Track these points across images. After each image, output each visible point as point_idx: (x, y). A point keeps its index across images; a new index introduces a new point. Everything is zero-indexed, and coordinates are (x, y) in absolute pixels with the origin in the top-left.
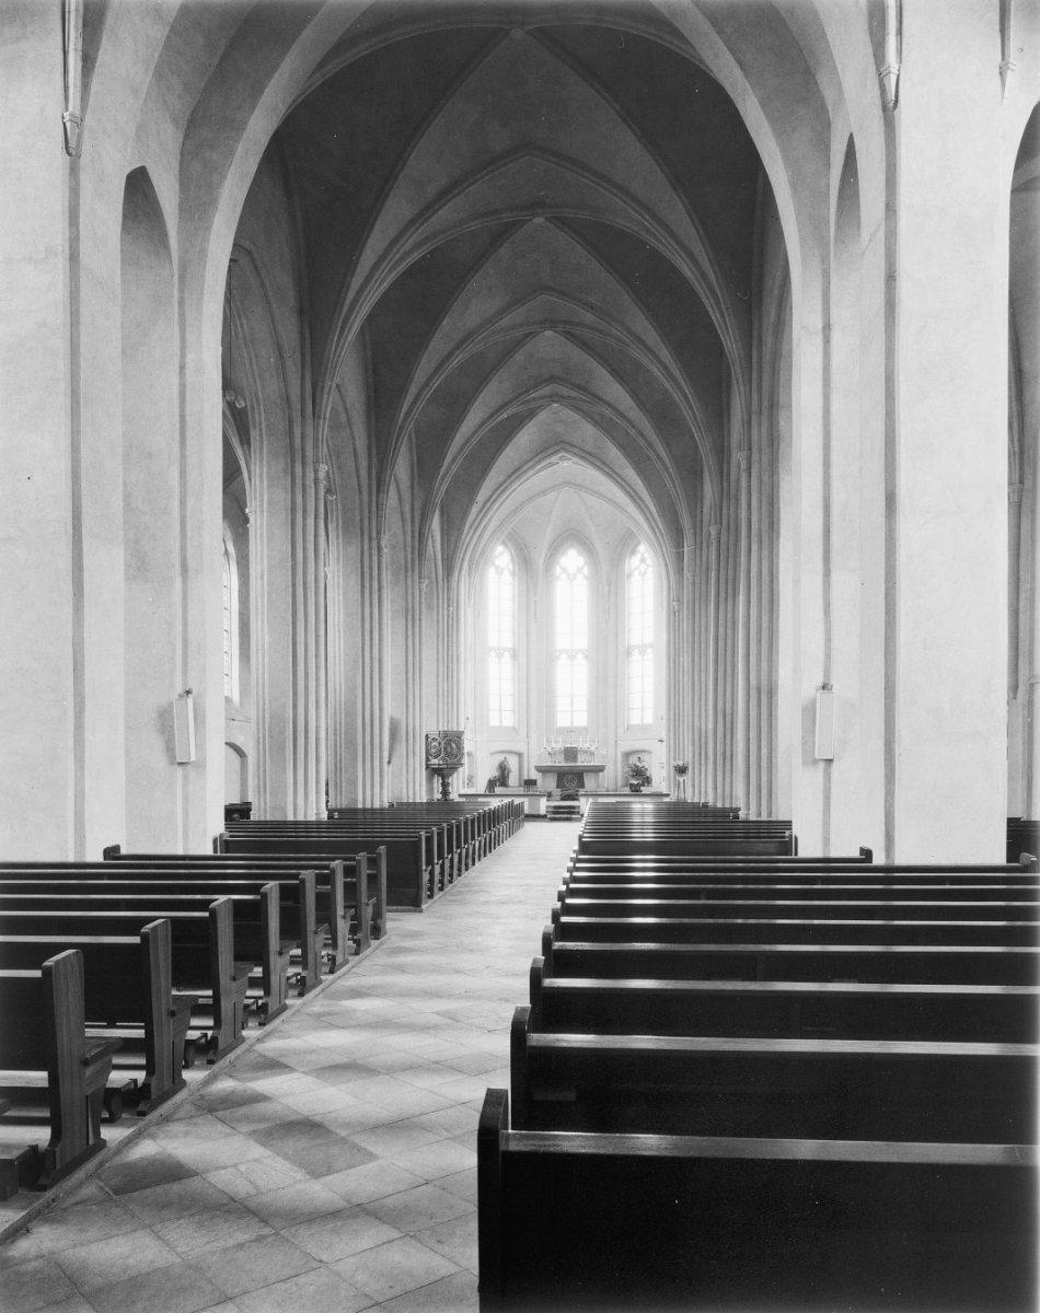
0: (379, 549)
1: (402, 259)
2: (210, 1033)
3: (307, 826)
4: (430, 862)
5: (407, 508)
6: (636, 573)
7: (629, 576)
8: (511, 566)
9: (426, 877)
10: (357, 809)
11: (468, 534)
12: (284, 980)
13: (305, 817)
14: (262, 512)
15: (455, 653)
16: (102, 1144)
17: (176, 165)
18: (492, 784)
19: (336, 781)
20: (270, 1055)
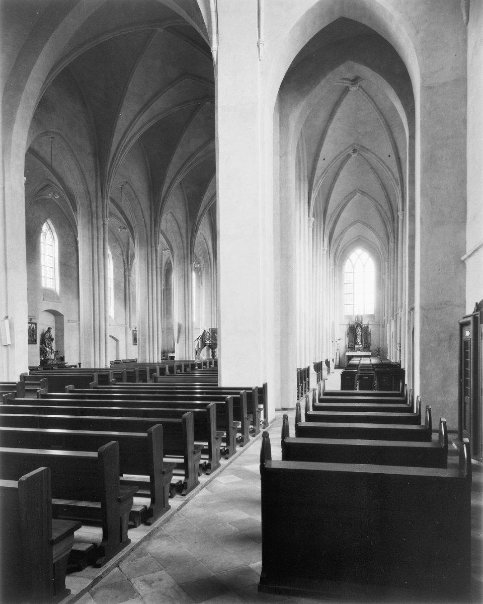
0: (156, 251)
13: (100, 366)
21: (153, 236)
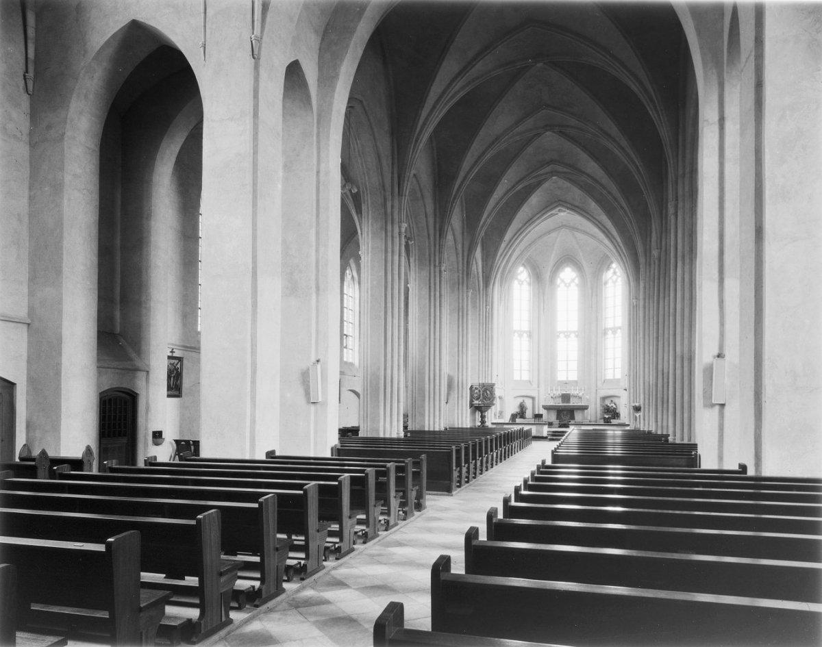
1: (452, 97)
2: (303, 562)
3: (392, 441)
4: (459, 465)
5: (460, 246)
6: (610, 281)
7: (606, 283)
8: (528, 280)
9: (455, 474)
10: (424, 431)
11: (499, 260)
12: (352, 534)
14: (368, 253)
15: (490, 335)
16: (230, 621)
17: (316, 57)
18: (514, 417)
19: (412, 414)
20: (338, 577)
21: (437, 254)
